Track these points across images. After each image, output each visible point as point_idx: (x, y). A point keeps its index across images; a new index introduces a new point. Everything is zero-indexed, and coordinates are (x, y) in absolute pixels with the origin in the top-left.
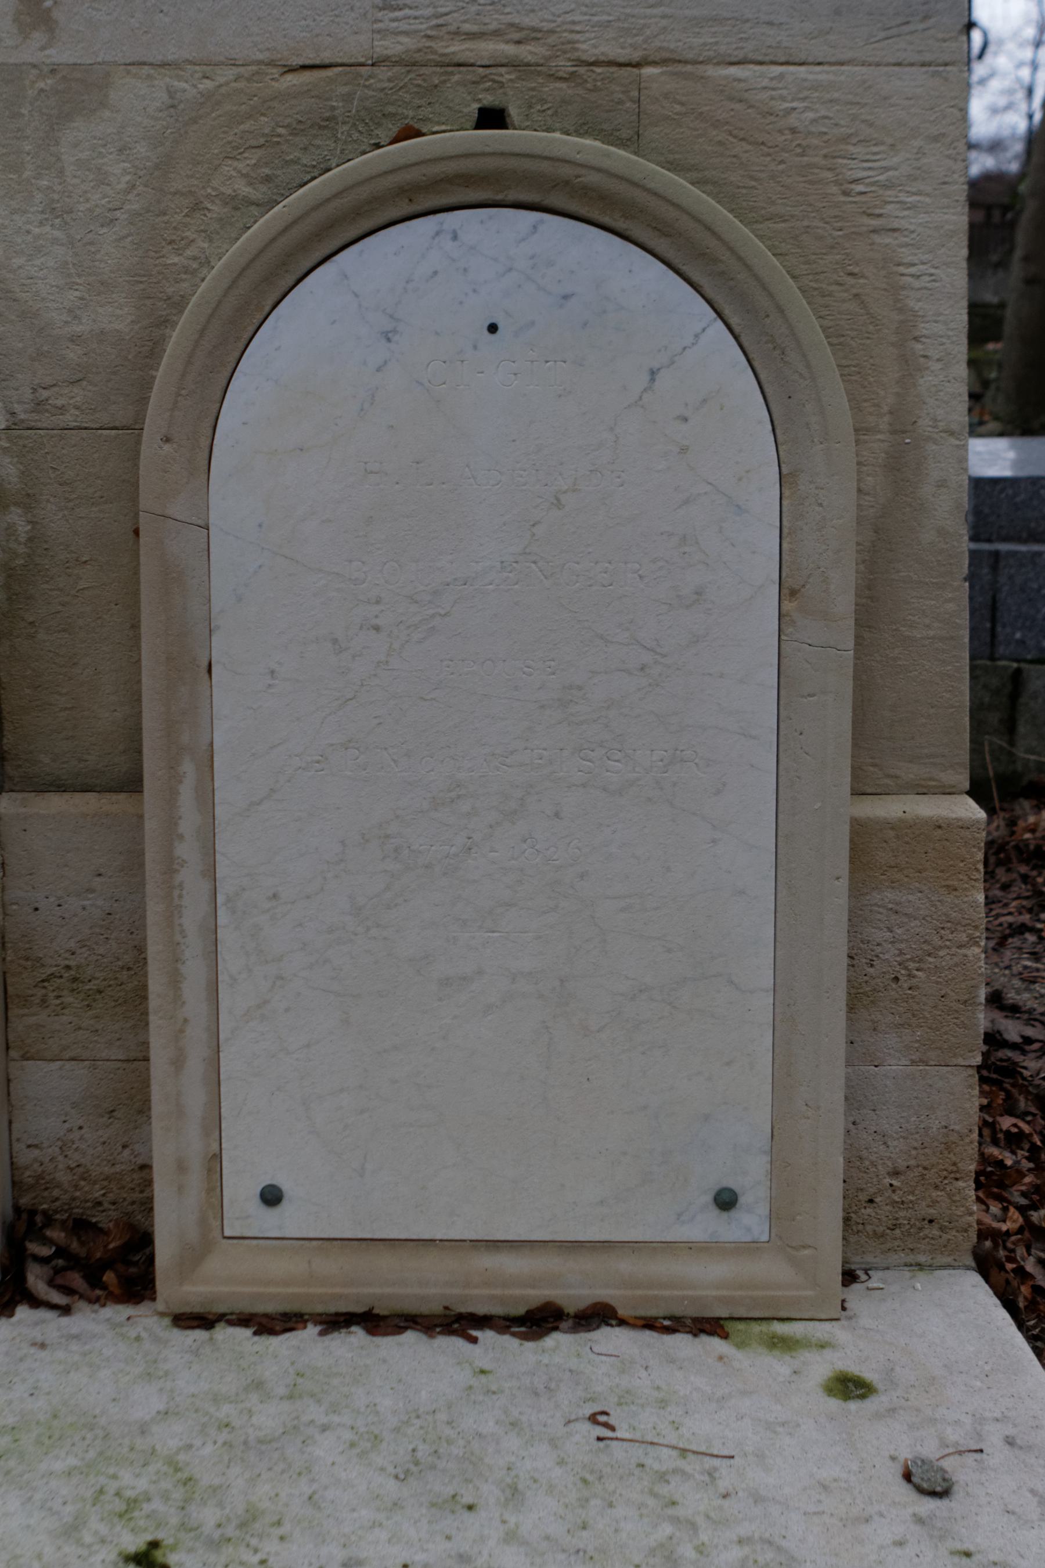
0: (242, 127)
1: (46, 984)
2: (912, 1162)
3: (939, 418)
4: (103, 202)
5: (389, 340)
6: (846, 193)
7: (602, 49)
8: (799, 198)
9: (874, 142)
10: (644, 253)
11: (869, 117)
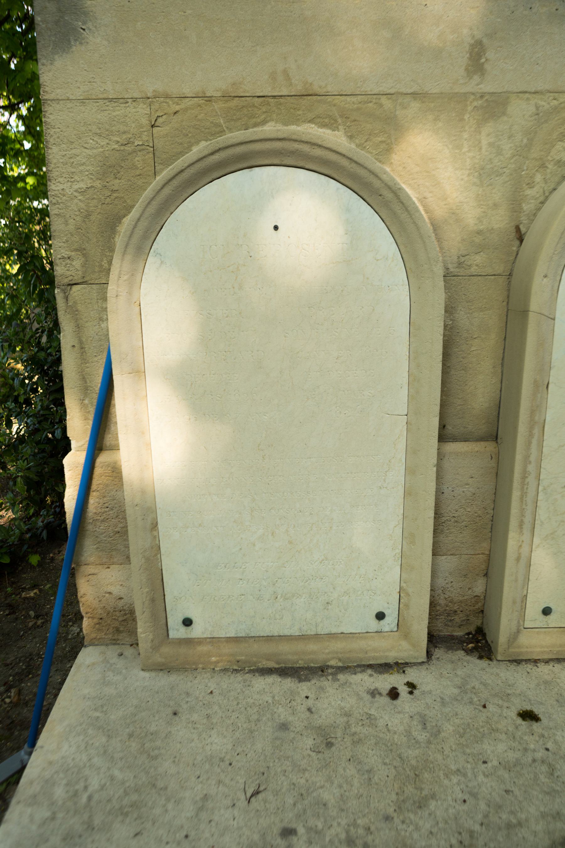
4: (499, 164)
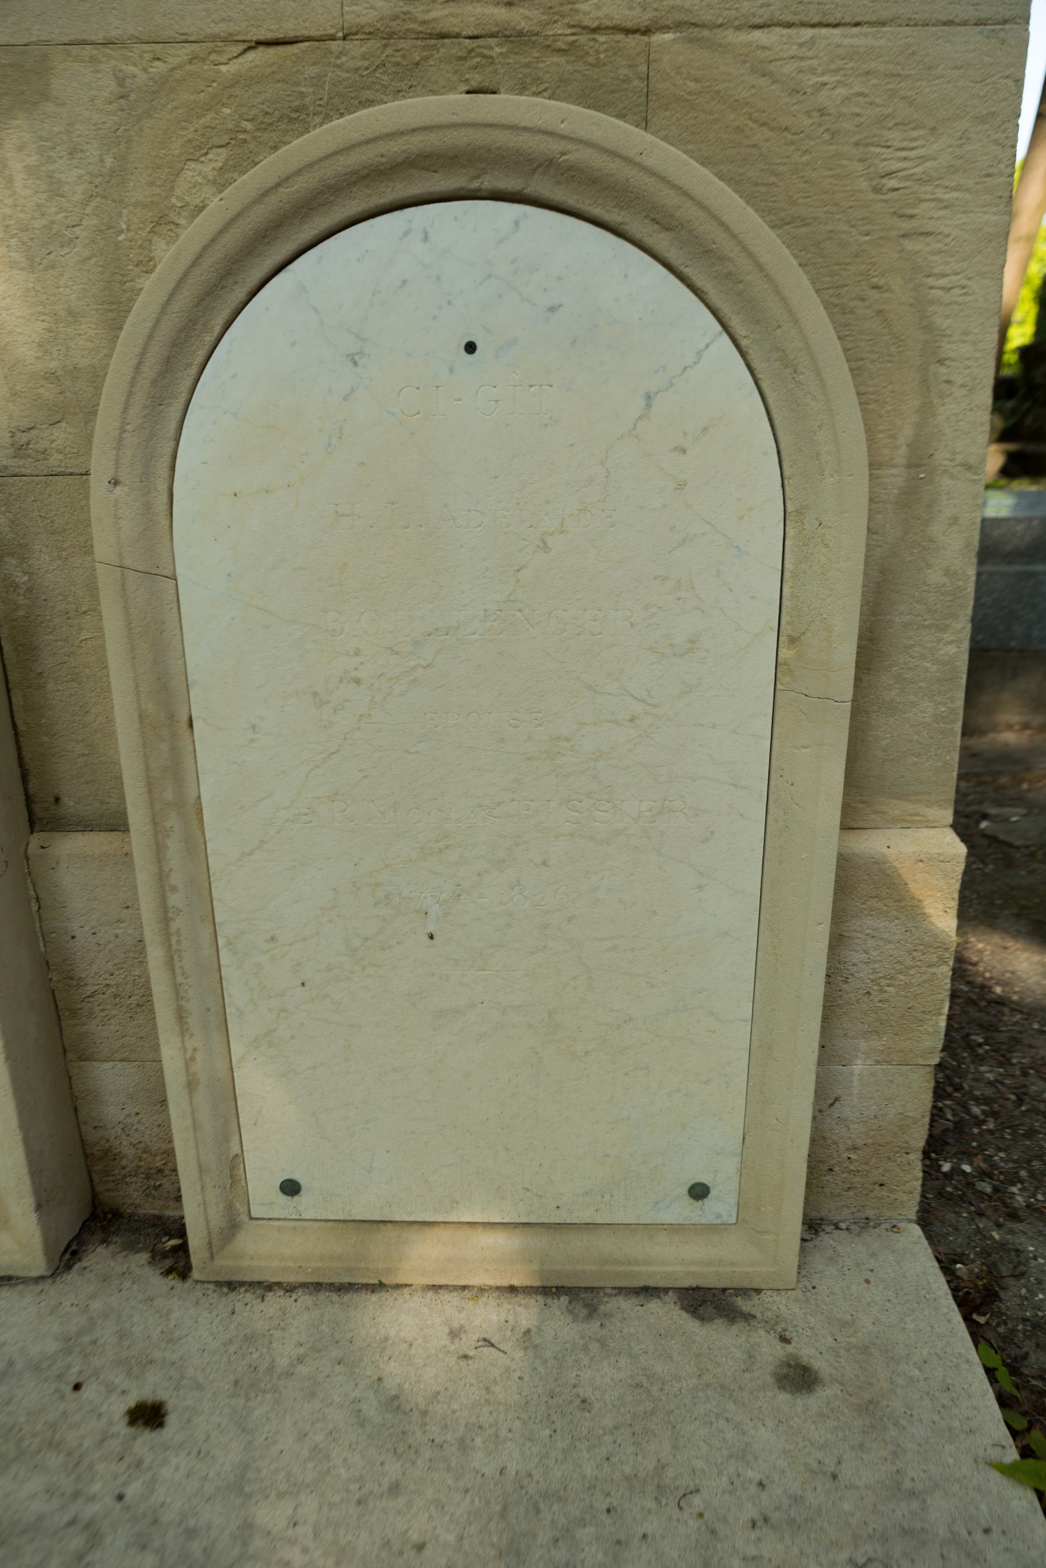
0: (202, 121)
1: (91, 999)
2: (870, 1141)
3: (958, 450)
4: (60, 216)
5: (355, 363)
6: (877, 190)
7: (606, 10)
8: (823, 196)
9: (912, 125)
10: (641, 254)
11: (909, 94)
